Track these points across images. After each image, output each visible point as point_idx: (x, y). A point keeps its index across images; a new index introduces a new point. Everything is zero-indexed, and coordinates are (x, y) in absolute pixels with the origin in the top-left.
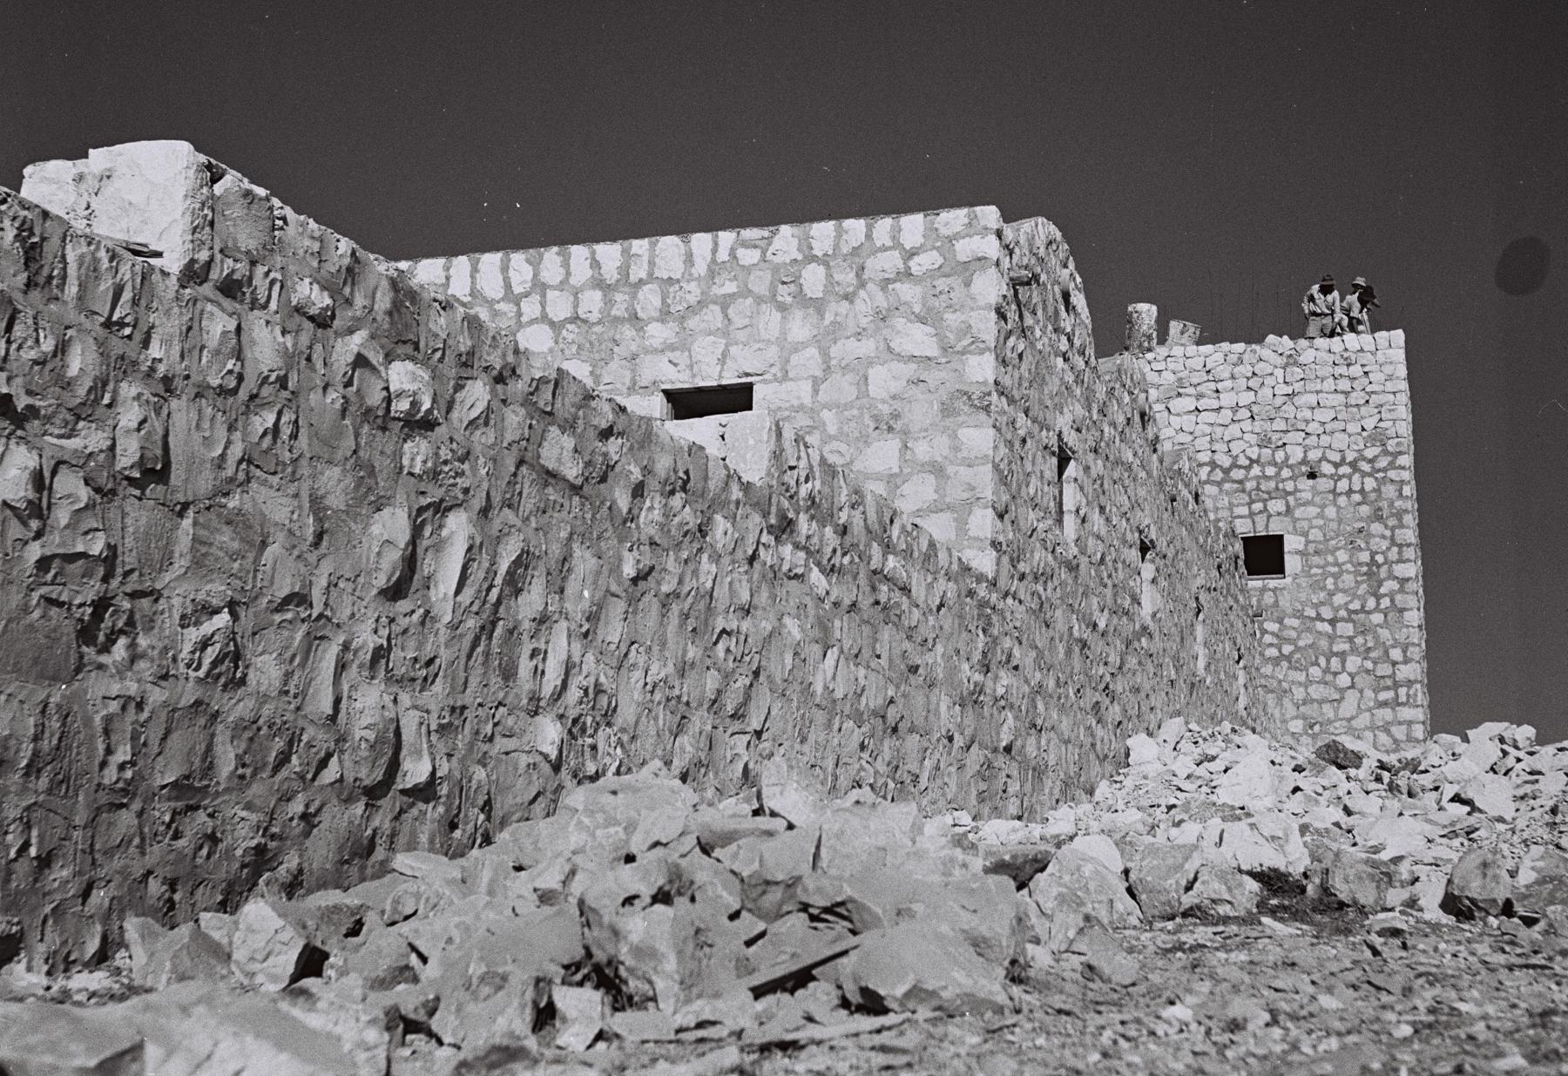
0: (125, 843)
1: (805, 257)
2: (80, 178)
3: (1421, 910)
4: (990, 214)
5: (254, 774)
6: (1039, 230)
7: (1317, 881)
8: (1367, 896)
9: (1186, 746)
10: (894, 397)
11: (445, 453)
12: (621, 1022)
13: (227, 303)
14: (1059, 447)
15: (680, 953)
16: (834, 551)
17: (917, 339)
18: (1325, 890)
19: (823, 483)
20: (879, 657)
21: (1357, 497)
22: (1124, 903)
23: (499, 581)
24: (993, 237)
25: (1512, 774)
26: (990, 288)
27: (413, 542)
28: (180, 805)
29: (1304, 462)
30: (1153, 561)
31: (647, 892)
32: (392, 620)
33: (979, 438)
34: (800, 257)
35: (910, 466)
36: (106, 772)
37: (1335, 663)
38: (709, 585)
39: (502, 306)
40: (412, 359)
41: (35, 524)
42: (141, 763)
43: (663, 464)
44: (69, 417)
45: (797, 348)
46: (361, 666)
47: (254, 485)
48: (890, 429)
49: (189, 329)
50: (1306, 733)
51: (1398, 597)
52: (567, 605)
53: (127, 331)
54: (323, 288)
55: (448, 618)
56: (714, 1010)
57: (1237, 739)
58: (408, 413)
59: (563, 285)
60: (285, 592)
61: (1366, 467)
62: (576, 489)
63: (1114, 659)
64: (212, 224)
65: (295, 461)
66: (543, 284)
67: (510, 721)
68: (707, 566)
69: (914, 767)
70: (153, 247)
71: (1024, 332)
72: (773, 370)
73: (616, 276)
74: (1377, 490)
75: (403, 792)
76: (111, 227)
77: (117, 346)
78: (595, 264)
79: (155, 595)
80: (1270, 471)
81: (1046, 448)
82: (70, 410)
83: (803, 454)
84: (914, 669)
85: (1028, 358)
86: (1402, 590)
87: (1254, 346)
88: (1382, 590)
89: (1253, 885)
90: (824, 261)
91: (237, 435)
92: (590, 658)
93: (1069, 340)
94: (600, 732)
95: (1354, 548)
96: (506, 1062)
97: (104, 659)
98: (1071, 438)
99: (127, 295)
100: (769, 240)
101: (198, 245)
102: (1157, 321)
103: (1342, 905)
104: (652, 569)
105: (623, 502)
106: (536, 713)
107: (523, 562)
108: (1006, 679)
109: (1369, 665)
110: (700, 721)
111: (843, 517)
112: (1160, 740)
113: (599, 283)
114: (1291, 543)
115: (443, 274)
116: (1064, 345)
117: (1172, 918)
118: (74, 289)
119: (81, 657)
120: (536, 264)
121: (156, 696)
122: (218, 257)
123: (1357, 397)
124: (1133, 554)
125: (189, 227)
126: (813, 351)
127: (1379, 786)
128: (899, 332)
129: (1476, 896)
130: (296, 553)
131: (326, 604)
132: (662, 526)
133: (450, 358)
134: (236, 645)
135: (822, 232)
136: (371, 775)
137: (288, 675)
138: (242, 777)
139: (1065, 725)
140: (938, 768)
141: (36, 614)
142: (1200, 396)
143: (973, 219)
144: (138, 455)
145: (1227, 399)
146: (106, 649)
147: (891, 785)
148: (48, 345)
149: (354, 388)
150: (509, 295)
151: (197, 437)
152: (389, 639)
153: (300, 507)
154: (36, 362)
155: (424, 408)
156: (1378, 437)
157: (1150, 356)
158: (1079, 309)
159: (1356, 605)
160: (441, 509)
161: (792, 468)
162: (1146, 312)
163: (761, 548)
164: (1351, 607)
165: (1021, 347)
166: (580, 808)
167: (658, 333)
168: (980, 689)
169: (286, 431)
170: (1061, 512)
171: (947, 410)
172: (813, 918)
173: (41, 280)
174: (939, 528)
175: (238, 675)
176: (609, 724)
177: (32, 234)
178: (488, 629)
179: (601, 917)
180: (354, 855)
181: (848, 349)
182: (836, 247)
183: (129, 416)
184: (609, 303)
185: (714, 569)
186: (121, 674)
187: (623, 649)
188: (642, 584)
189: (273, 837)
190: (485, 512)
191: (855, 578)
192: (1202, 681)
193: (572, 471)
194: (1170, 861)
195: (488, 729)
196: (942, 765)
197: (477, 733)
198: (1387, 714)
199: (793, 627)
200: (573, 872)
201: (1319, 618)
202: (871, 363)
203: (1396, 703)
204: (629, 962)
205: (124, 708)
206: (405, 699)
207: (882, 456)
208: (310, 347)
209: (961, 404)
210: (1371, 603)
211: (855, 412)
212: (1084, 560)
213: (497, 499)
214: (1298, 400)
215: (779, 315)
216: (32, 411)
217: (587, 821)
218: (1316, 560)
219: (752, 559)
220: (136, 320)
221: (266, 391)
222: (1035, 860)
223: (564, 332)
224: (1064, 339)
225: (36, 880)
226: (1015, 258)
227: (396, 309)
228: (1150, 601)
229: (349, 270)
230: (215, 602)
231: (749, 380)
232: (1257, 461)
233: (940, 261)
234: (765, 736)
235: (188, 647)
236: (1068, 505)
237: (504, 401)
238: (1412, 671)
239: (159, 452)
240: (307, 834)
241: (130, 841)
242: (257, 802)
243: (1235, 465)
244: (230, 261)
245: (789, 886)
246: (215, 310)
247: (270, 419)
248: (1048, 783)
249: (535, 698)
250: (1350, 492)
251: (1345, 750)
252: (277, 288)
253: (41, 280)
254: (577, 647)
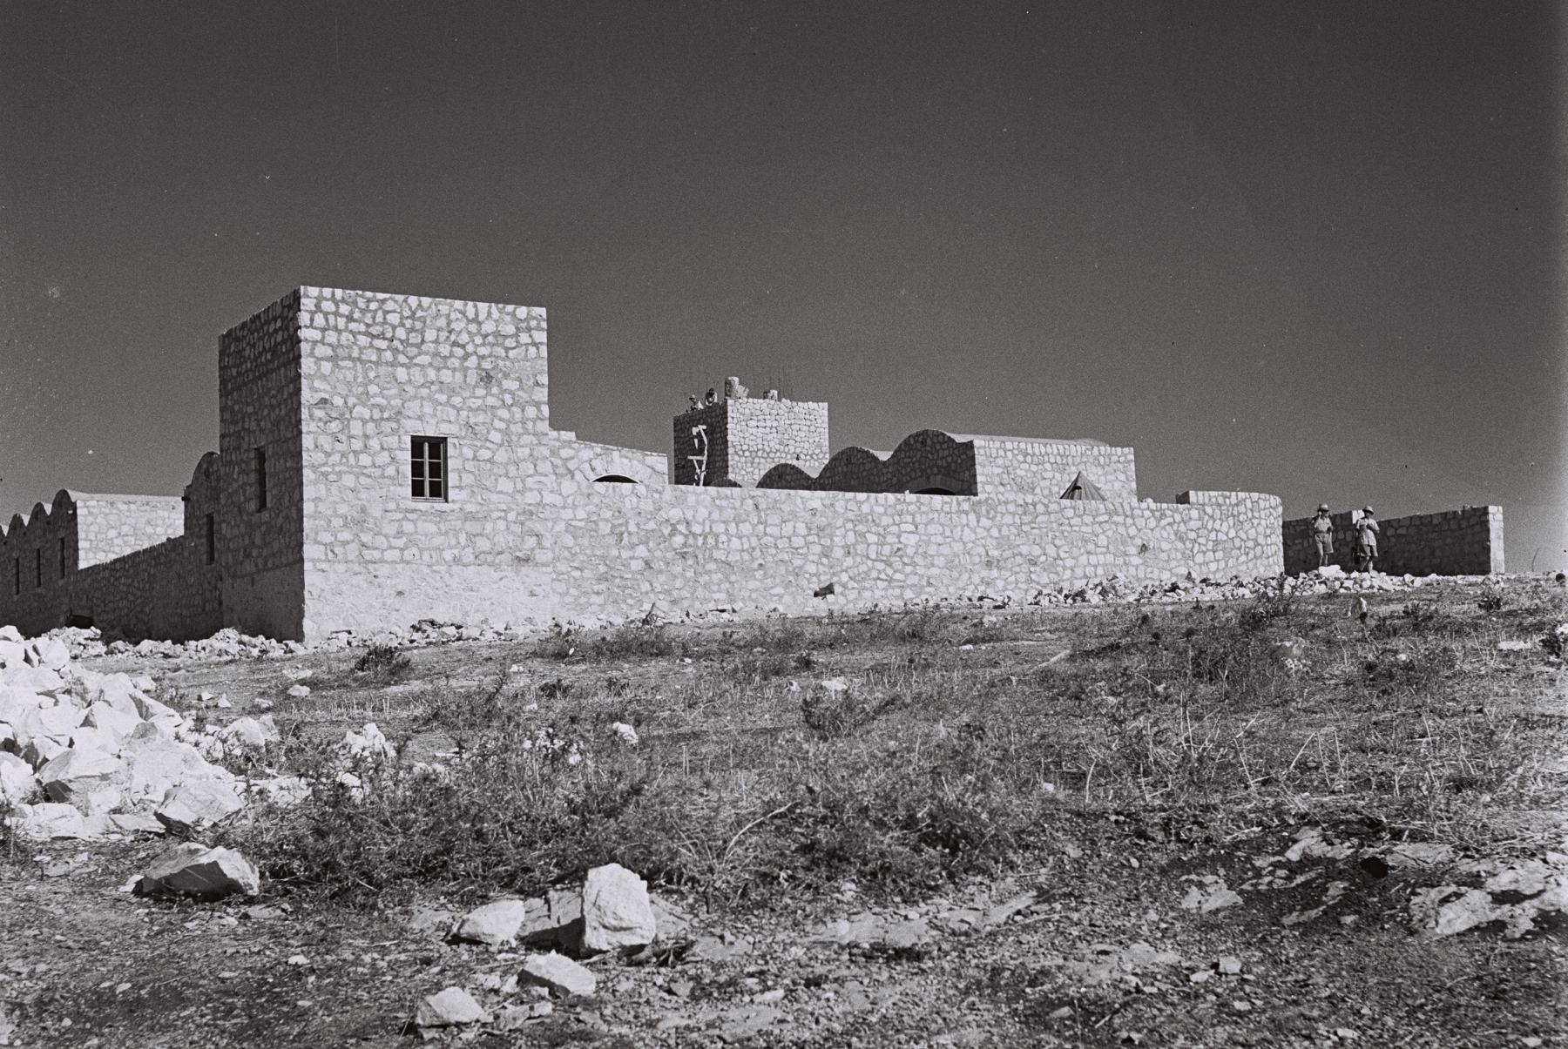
123: (812, 428)
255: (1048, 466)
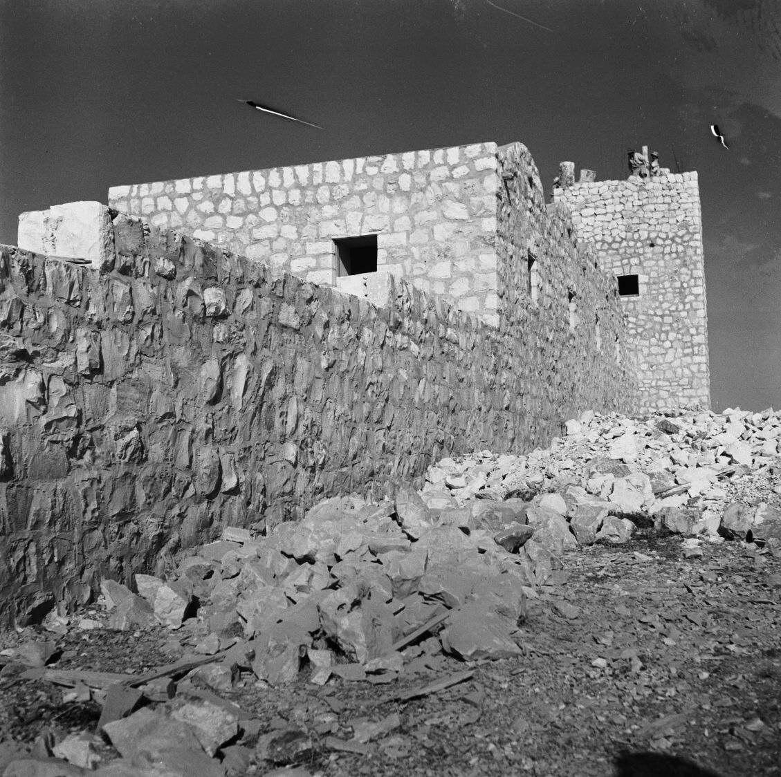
0: (98, 545)
1: (400, 170)
2: (47, 221)
3: (708, 535)
4: (492, 146)
5: (155, 501)
6: (517, 148)
7: (659, 520)
8: (683, 528)
9: (594, 425)
10: (447, 240)
11: (233, 329)
12: (339, 670)
13: (125, 279)
14: (529, 256)
15: (366, 634)
16: (422, 333)
17: (457, 211)
18: (663, 526)
19: (415, 300)
20: (444, 378)
21: (674, 255)
22: (569, 539)
23: (263, 384)
24: (494, 158)
25: (752, 440)
26: (493, 184)
27: (221, 375)
28: (121, 522)
29: (648, 238)
30: (575, 302)
31: (349, 602)
32: (213, 414)
33: (489, 259)
34: (398, 171)
35: (456, 274)
36: (86, 515)
37: (663, 336)
38: (362, 363)
39: (250, 199)
40: (215, 285)
41: (42, 408)
42: (102, 507)
43: (338, 309)
44: (53, 352)
45: (398, 216)
46: (201, 439)
47: (144, 364)
48: (446, 256)
49: (107, 295)
50: (649, 370)
51: (694, 304)
52: (296, 388)
53: (78, 304)
54: (170, 260)
55: (240, 407)
56: (384, 663)
57: (619, 421)
58: (215, 313)
59: (281, 187)
60: (161, 414)
61: (678, 240)
62: (297, 331)
63: (557, 353)
64: (114, 241)
65: (162, 348)
66: (270, 187)
67: (272, 449)
68: (361, 353)
69: (463, 427)
70: (87, 259)
71: (510, 202)
72: (387, 228)
73: (307, 182)
74: (684, 252)
75: (224, 493)
76: (64, 252)
77: (74, 312)
78: (296, 177)
79: (102, 427)
80: (632, 244)
81: (522, 258)
82: (53, 348)
83: (405, 289)
84: (461, 380)
85: (513, 215)
86: (696, 300)
87: (623, 182)
88: (686, 300)
89: (628, 524)
90: (410, 172)
91: (134, 342)
92: (308, 410)
93: (532, 201)
94: (315, 444)
95: (672, 280)
96: (294, 739)
97: (81, 462)
98: (534, 251)
99: (76, 286)
100: (382, 162)
101: (107, 253)
102: (575, 170)
103: (672, 533)
104: (335, 362)
105: (319, 332)
106: (284, 442)
107: (273, 373)
108: (505, 375)
109: (680, 336)
110: (362, 428)
111: (425, 316)
112: (582, 421)
113: (298, 186)
114: (642, 279)
115: (220, 183)
116: (530, 205)
117: (591, 545)
118: (51, 289)
119: (70, 464)
120: (266, 177)
121: (106, 475)
122: (118, 256)
124: (566, 300)
125: (103, 245)
126: (405, 218)
127: (687, 446)
128: (448, 207)
129: (734, 529)
130: (166, 392)
131: (182, 414)
132: (338, 340)
133: (233, 280)
134: (142, 443)
135: (408, 157)
136: (208, 489)
137: (167, 451)
138: (149, 503)
139: (534, 391)
140: (474, 424)
141: (47, 450)
142: (596, 207)
143: (483, 149)
144: (88, 364)
145: (610, 209)
146: (81, 457)
147: (453, 438)
148: (41, 319)
149: (188, 307)
150: (254, 192)
151: (115, 348)
152: (213, 424)
153: (166, 370)
154: (35, 329)
155: (222, 309)
156: (685, 225)
157: (571, 188)
158: (537, 185)
159: (673, 308)
160: (233, 356)
161: (399, 297)
162: (569, 166)
163: (387, 339)
164: (671, 309)
165: (509, 211)
166: (312, 530)
167: (329, 211)
168: (493, 382)
169: (157, 335)
170: (530, 287)
171: (473, 246)
172: (426, 599)
173: (34, 288)
174: (469, 306)
175: (144, 456)
176: (318, 439)
177: (28, 266)
178: (259, 409)
179: (328, 616)
180: (203, 527)
181: (423, 216)
182: (416, 165)
183: (82, 345)
184: (303, 195)
185: (364, 354)
186: (89, 468)
187: (323, 403)
188: (331, 370)
189: (166, 528)
190: (254, 353)
191: (432, 343)
192: (600, 354)
193: (294, 323)
194: (589, 515)
195: (262, 455)
196: (476, 422)
197: (257, 457)
198: (688, 359)
199: (403, 374)
200: (312, 575)
201: (655, 315)
202: (434, 223)
203: (693, 354)
204: (343, 637)
205: (92, 484)
206: (223, 450)
207: (442, 269)
208: (166, 291)
209: (480, 243)
210: (681, 307)
211: (427, 248)
212: (541, 309)
213: (259, 345)
214: (645, 208)
215: (388, 200)
216: (36, 353)
217: (316, 537)
218: (654, 287)
219: (382, 346)
220: (82, 298)
221: (146, 318)
222: (527, 534)
223: (282, 211)
224: (530, 201)
225: (58, 573)
226: (505, 166)
227: (206, 261)
228: (573, 320)
229: (182, 249)
230: (130, 426)
231: (375, 233)
232: (625, 239)
233: (468, 171)
234: (392, 428)
235: (119, 449)
236: (534, 283)
237: (260, 296)
238: (701, 338)
239: (98, 360)
240: (181, 522)
241: (100, 545)
242: (157, 513)
243: (614, 241)
244: (124, 258)
245: (414, 581)
246: (119, 283)
247: (149, 331)
248: (527, 420)
249: (283, 436)
250: (671, 253)
251: (670, 425)
252: (147, 266)
253: (34, 288)
254: (301, 406)
255: (269, 214)
